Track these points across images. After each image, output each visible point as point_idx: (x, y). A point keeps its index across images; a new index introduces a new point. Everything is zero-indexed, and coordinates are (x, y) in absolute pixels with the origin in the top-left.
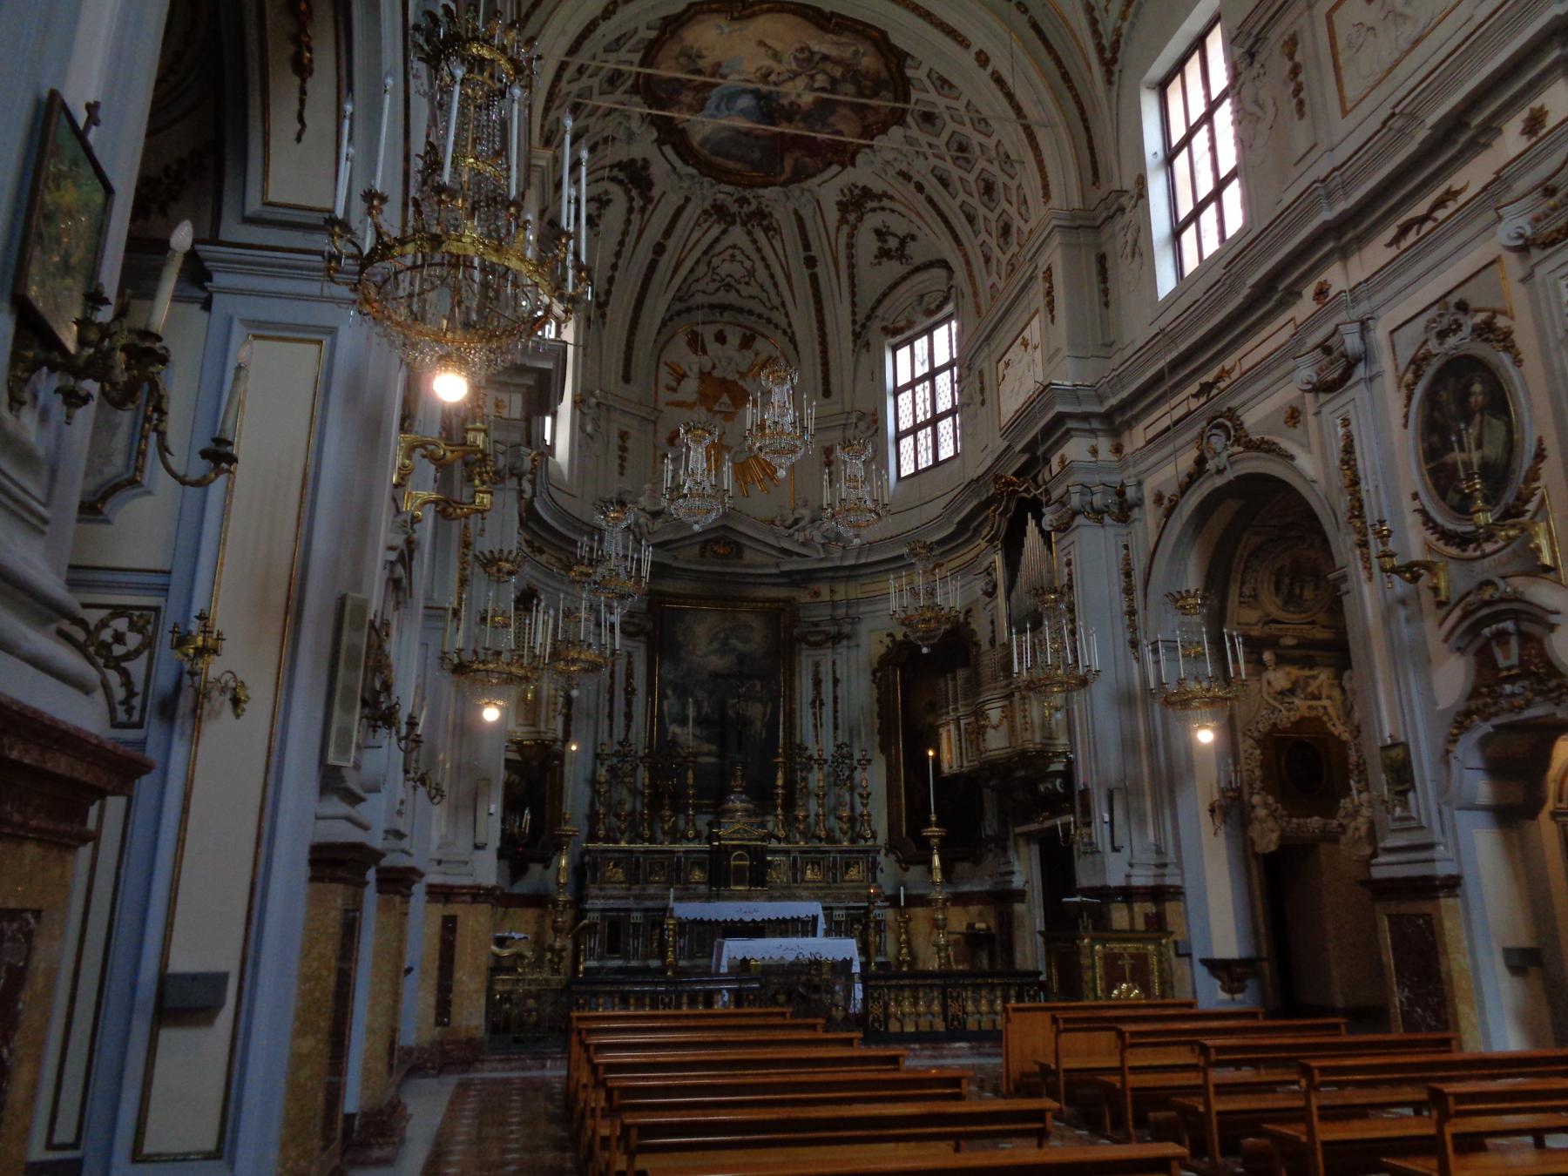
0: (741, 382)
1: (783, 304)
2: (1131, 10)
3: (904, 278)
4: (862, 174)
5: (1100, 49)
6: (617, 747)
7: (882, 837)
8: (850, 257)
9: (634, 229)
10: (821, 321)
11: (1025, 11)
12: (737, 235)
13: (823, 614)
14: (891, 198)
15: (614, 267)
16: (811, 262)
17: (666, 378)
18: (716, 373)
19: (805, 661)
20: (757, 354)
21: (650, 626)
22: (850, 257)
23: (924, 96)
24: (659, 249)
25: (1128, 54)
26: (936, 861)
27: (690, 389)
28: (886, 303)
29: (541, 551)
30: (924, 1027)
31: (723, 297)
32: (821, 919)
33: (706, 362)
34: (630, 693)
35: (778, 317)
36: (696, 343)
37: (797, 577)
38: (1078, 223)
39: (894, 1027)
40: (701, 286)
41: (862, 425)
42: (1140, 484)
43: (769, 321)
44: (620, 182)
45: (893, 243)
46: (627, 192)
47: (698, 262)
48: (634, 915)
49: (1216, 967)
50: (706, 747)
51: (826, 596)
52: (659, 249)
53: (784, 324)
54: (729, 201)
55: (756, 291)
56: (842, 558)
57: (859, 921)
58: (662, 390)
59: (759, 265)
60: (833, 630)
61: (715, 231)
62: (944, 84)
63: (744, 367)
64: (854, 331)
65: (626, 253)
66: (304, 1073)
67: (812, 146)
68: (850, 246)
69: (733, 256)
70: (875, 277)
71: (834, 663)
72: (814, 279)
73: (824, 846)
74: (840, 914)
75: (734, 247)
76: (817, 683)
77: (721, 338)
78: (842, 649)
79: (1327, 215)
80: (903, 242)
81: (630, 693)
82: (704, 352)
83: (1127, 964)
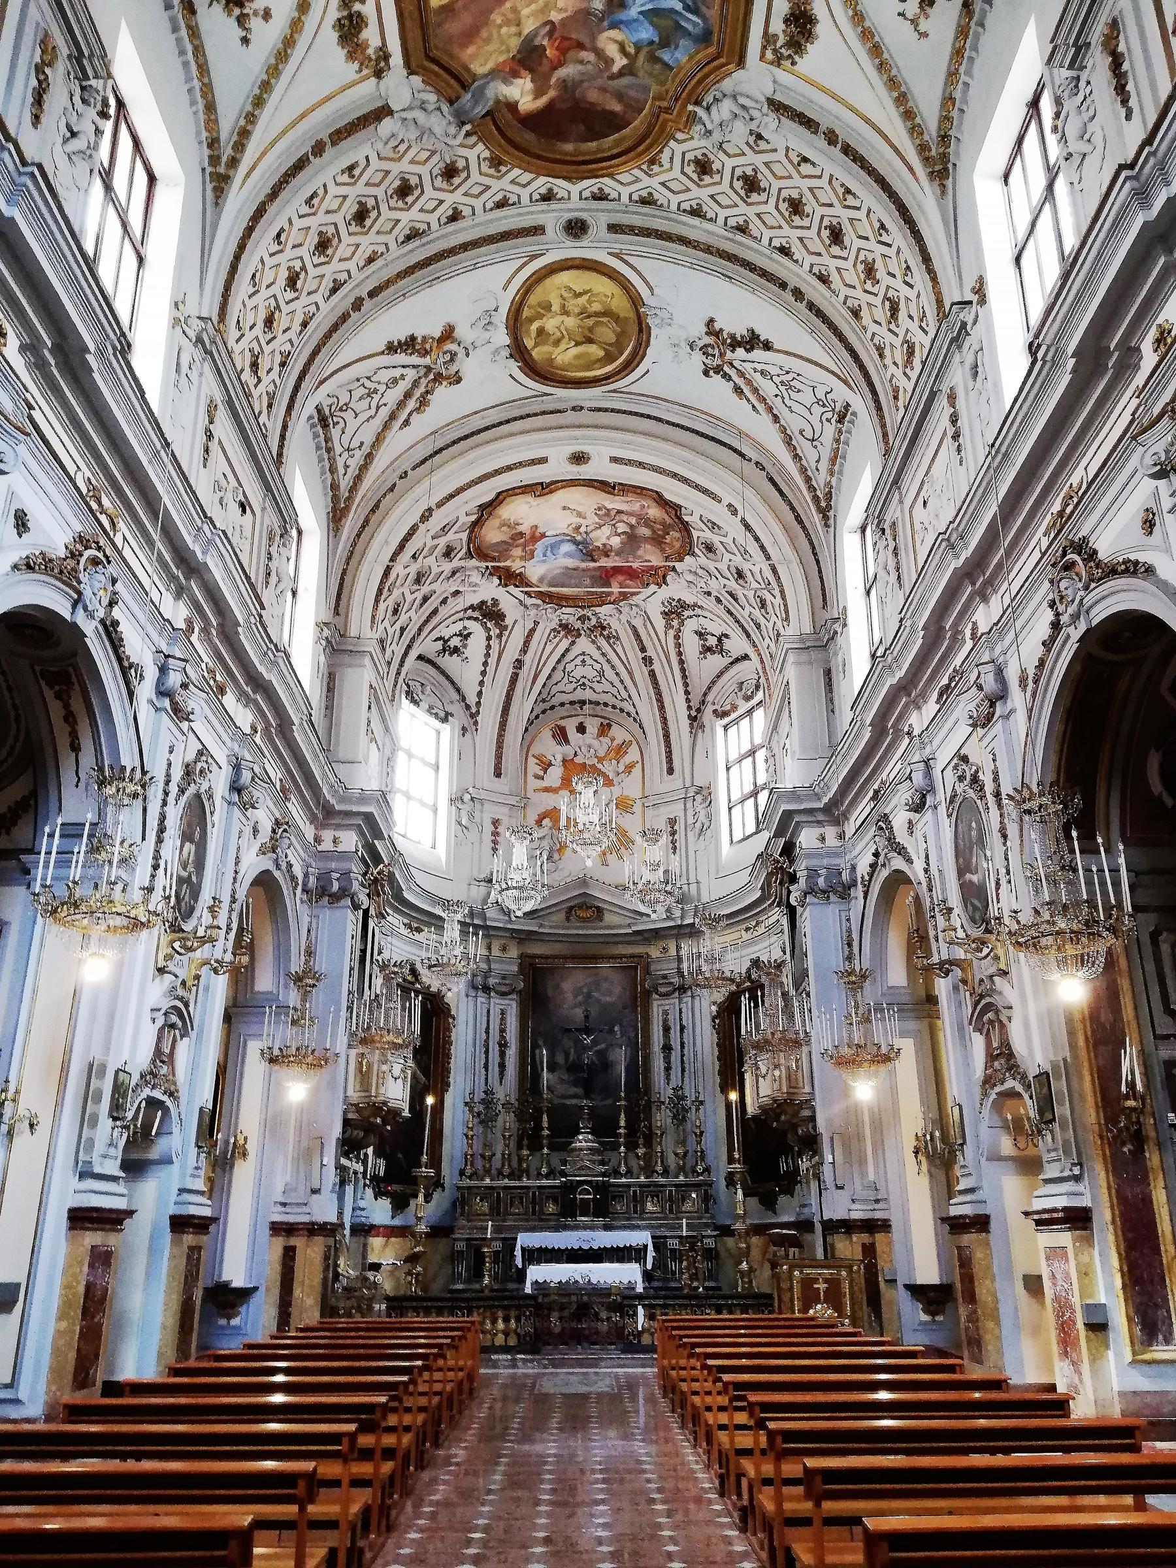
2: (836, 468)
3: (727, 668)
4: (676, 589)
5: (816, 499)
8: (680, 654)
9: (494, 653)
10: (662, 708)
11: (763, 469)
12: (583, 644)
13: (669, 968)
14: (700, 607)
15: (482, 683)
16: (648, 661)
17: (534, 768)
19: (657, 1007)
20: (613, 740)
22: (680, 654)
23: (701, 534)
24: (519, 664)
25: (838, 501)
27: (555, 776)
28: (715, 689)
29: (419, 930)
31: (580, 695)
33: (568, 750)
34: (503, 1046)
35: (628, 707)
36: (561, 735)
38: (808, 644)
40: (560, 687)
41: (699, 798)
42: (853, 868)
43: (622, 710)
44: (476, 619)
45: (712, 641)
46: (484, 625)
47: (554, 669)
49: (918, 1291)
50: (574, 1090)
52: (519, 664)
53: (632, 711)
54: (572, 620)
55: (608, 687)
56: (682, 918)
58: (530, 778)
59: (607, 667)
61: (565, 644)
62: (713, 526)
63: (601, 753)
64: (689, 716)
65: (490, 669)
66: (62, 1342)
67: (631, 574)
68: (678, 645)
69: (583, 661)
70: (704, 668)
72: (652, 674)
73: (661, 1180)
74: (673, 1243)
75: (583, 654)
76: (667, 1029)
77: (581, 729)
79: (892, 680)
80: (720, 640)
81: (503, 1046)
82: (567, 741)
83: (822, 1286)
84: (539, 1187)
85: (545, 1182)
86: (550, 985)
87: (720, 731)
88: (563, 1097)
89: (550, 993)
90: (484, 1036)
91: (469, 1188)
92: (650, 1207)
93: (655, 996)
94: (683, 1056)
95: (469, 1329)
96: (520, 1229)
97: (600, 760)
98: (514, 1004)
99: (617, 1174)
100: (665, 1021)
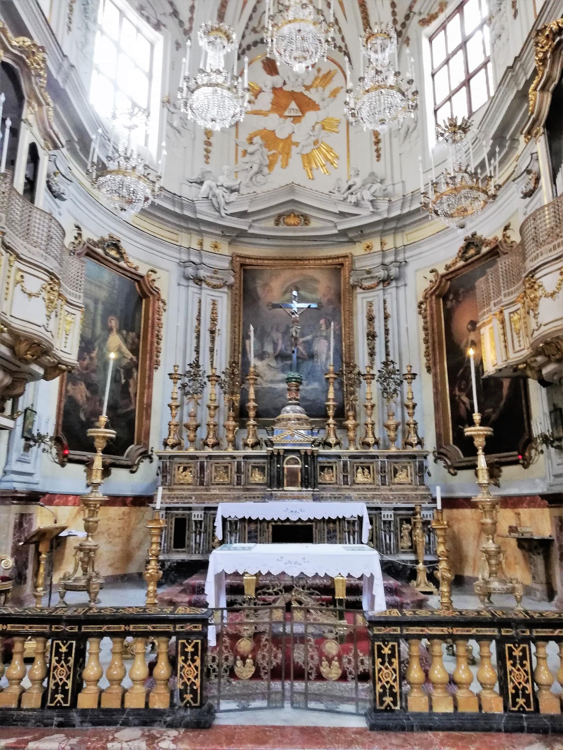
0: (306, 93)
1: (336, 21)
6: (188, 368)
7: (430, 444)
18: (286, 88)
19: (361, 301)
21: (232, 280)
26: (461, 371)
30: (469, 707)
32: (366, 521)
33: (277, 80)
37: (351, 235)
39: (417, 703)
48: (194, 513)
51: (377, 247)
56: (389, 210)
57: (408, 521)
60: (382, 274)
63: (308, 83)
71: (385, 302)
74: (387, 515)
76: (371, 319)
78: (391, 289)
84: (245, 457)
85: (249, 452)
86: (259, 283)
87: (425, 42)
88: (272, 382)
89: (260, 291)
90: (195, 323)
91: (171, 457)
92: (360, 478)
93: (359, 290)
94: (387, 342)
96: (222, 498)
97: (308, 88)
98: (225, 296)
99: (326, 444)
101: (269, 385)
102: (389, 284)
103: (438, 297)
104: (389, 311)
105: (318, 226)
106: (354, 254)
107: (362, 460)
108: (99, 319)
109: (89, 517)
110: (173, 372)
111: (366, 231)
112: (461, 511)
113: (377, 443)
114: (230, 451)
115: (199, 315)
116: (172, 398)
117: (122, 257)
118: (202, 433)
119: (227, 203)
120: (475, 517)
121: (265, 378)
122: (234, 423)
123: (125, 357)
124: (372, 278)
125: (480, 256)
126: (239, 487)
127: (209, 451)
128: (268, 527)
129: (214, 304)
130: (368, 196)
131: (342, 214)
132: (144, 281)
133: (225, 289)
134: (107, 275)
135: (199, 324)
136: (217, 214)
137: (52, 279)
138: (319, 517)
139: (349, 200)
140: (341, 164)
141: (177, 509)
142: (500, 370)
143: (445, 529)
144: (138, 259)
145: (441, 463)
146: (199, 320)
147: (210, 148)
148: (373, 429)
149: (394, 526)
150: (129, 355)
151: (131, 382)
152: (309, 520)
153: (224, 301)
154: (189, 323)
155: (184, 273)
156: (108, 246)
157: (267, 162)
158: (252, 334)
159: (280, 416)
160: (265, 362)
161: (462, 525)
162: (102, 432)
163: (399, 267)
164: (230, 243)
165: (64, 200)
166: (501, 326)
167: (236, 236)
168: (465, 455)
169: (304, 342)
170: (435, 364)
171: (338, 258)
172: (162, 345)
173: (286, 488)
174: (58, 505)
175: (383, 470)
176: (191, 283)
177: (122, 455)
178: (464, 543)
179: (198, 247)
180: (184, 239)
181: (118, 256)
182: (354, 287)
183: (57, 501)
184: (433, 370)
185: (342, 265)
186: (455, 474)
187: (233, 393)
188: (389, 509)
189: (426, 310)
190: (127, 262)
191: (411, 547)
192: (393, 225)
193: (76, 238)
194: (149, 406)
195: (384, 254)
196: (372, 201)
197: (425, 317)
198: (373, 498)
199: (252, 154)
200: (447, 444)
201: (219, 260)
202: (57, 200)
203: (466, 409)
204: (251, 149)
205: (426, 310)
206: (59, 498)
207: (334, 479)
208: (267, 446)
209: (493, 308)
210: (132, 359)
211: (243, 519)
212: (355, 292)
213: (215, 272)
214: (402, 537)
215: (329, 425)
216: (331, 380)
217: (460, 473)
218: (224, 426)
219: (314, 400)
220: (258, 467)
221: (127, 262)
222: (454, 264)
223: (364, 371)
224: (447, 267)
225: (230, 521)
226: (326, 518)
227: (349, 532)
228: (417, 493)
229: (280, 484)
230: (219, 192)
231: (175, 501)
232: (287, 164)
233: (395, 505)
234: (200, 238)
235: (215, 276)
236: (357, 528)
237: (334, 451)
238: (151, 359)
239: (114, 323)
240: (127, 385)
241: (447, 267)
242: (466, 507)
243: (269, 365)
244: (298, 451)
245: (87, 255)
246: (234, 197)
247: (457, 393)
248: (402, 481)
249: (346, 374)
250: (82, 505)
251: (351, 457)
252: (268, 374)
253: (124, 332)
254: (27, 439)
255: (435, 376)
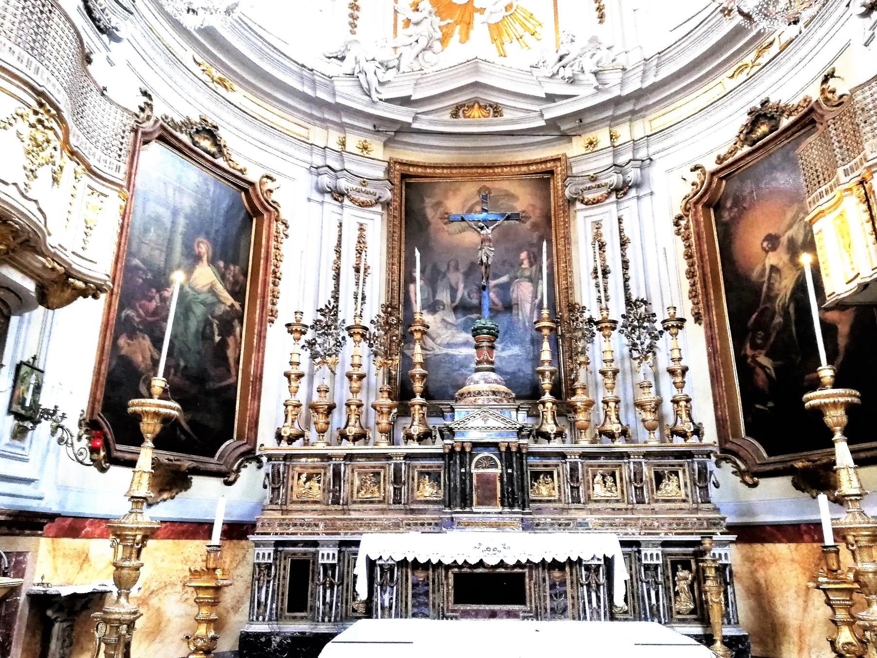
7: (710, 435)
19: (582, 223)
21: (388, 195)
48: (323, 551)
56: (622, 84)
57: (686, 566)
60: (615, 179)
74: (652, 554)
78: (630, 202)
84: (408, 457)
85: (414, 447)
88: (449, 345)
90: (334, 256)
92: (599, 491)
93: (579, 206)
94: (626, 280)
95: (479, 363)
96: (369, 525)
98: (378, 218)
100: (597, 236)
101: (445, 351)
102: (625, 194)
103: (707, 206)
104: (627, 233)
105: (516, 117)
106: (569, 155)
107: (602, 461)
108: (178, 241)
109: (124, 559)
110: (293, 321)
111: (588, 120)
112: (770, 547)
113: (624, 433)
114: (384, 447)
115: (339, 245)
116: (291, 363)
117: (220, 151)
118: (338, 419)
119: (381, 84)
120: (796, 557)
121: (438, 341)
122: (389, 402)
123: (220, 302)
124: (599, 186)
125: (776, 133)
126: (397, 506)
127: (347, 447)
128: (447, 577)
129: (361, 229)
130: (590, 65)
131: (551, 98)
132: (255, 189)
133: (378, 208)
134: (192, 175)
135: (339, 258)
136: (368, 98)
137: (41, 105)
138: (537, 560)
139: (561, 74)
140: (547, 32)
141: (295, 544)
142: (865, 286)
143: (850, 591)
144: (245, 158)
145: (728, 467)
146: (338, 252)
147: (356, 13)
148: (617, 410)
149: (663, 574)
150: (229, 300)
151: (231, 340)
152: (519, 564)
153: (377, 227)
154: (326, 256)
155: (317, 183)
156: (198, 131)
157: (439, 35)
158: (417, 274)
159: (464, 390)
160: (438, 316)
161: (773, 570)
162: (155, 405)
163: (641, 168)
164: (385, 145)
165: (118, 40)
166: (865, 207)
167: (394, 132)
168: (770, 455)
169: (496, 286)
170: (708, 308)
171: (545, 162)
172: (282, 286)
173: (475, 510)
174: (88, 536)
175: (638, 476)
176: (328, 198)
177: (213, 456)
178: (778, 600)
179: (338, 148)
180: (318, 135)
181: (213, 149)
182: (571, 202)
183: (88, 529)
184: (704, 319)
185: (551, 172)
186: (755, 485)
187: (388, 355)
188: (654, 545)
189: (687, 228)
190: (228, 160)
191: (693, 612)
192: (628, 107)
193: (142, 110)
194: (259, 378)
195: (616, 150)
196: (596, 74)
197: (687, 239)
198: (626, 525)
199: (417, 24)
200: (736, 434)
201: (372, 166)
202: (105, 37)
203: (768, 376)
204: (415, 17)
205: (687, 228)
206: (91, 524)
207: (556, 493)
208: (443, 438)
209: (843, 179)
210: (232, 306)
211: (403, 563)
212: (572, 210)
213: (364, 184)
214: (677, 594)
215: (543, 403)
216: (546, 332)
217: (763, 482)
218: (374, 407)
219: (514, 373)
220: (428, 473)
221: (228, 160)
222: (731, 153)
223: (597, 317)
224: (720, 160)
225: (381, 566)
226: (549, 560)
227: (589, 585)
228: (700, 515)
229: (466, 501)
230: (370, 68)
231: (292, 530)
232: (467, 38)
233: (663, 537)
234: (342, 135)
235: (364, 189)
236: (602, 579)
237: (555, 445)
238: (263, 306)
239: (204, 248)
240: (223, 344)
241: (720, 160)
242: (780, 542)
243: (443, 320)
244: (496, 445)
245: (161, 138)
246: (391, 75)
247: (749, 352)
248: (673, 495)
249: (566, 326)
250: (112, 537)
251: (584, 456)
252: (445, 336)
253: (221, 264)
254: (18, 416)
255: (709, 326)
